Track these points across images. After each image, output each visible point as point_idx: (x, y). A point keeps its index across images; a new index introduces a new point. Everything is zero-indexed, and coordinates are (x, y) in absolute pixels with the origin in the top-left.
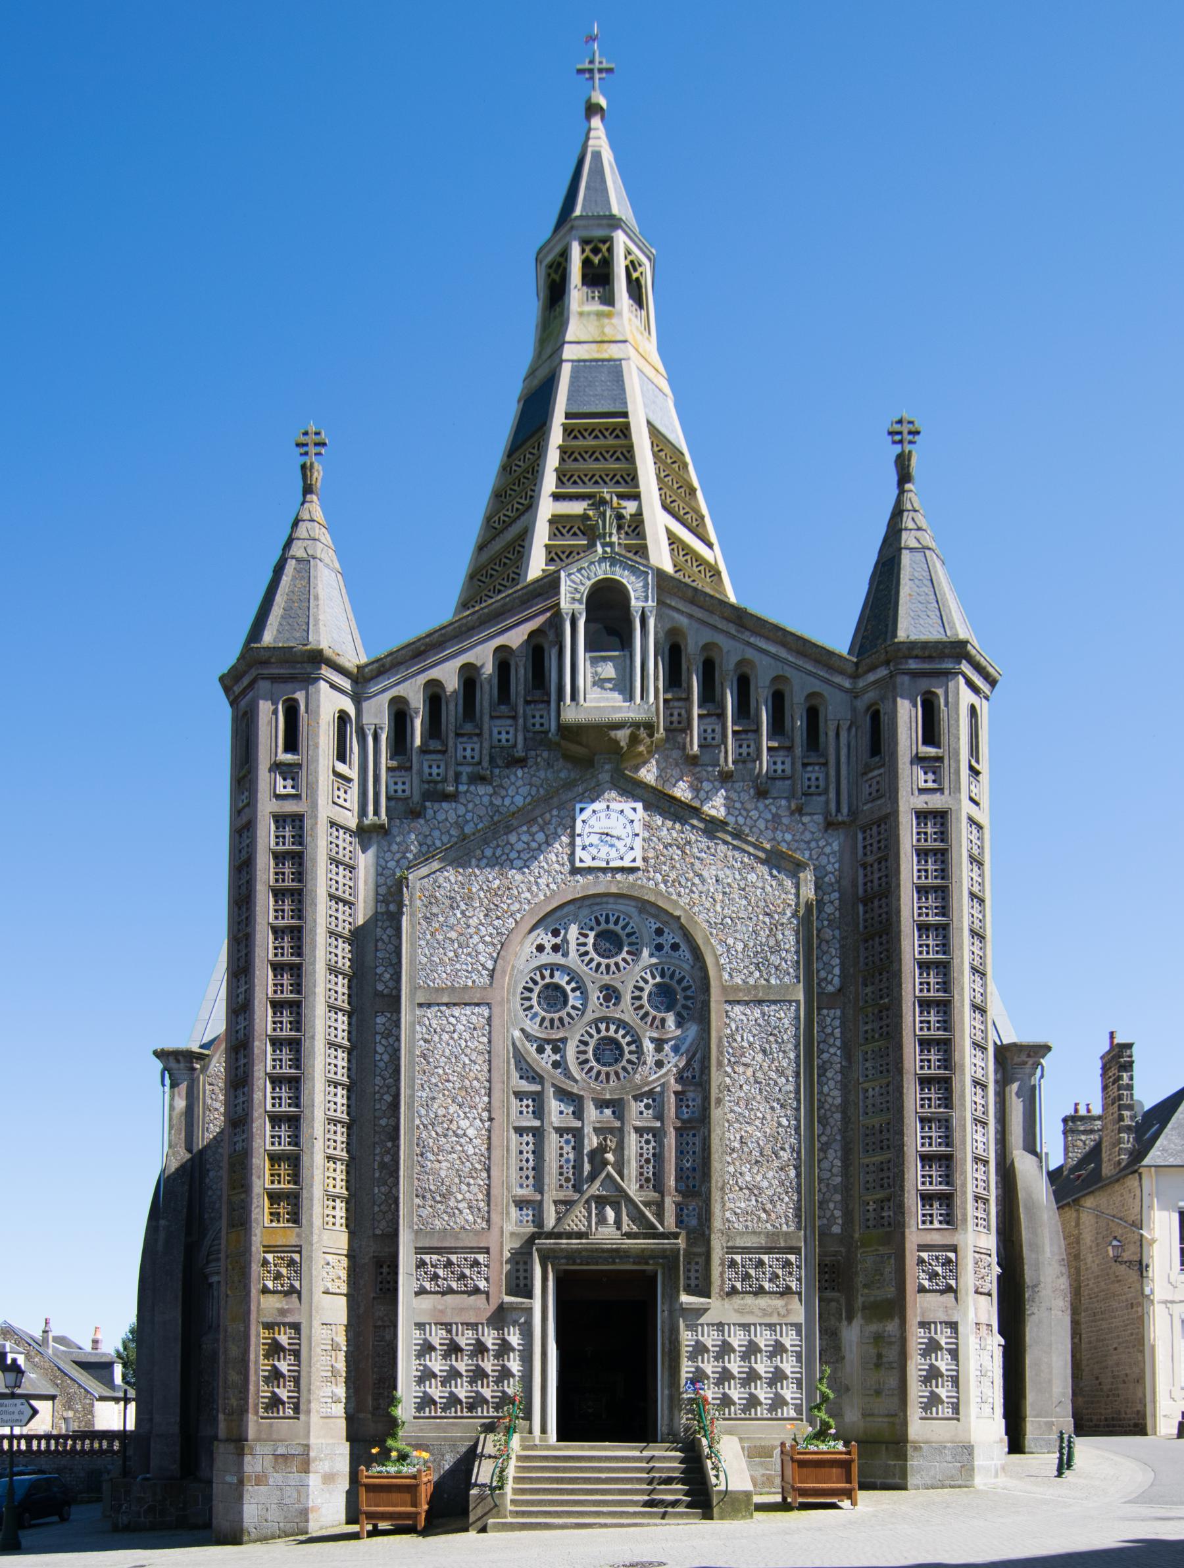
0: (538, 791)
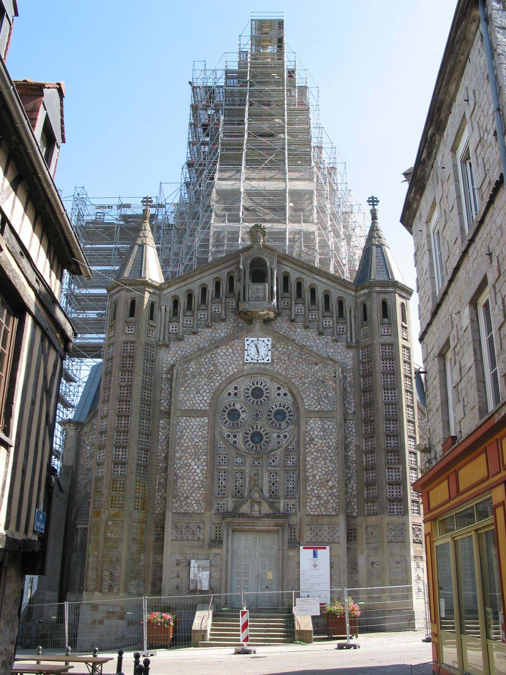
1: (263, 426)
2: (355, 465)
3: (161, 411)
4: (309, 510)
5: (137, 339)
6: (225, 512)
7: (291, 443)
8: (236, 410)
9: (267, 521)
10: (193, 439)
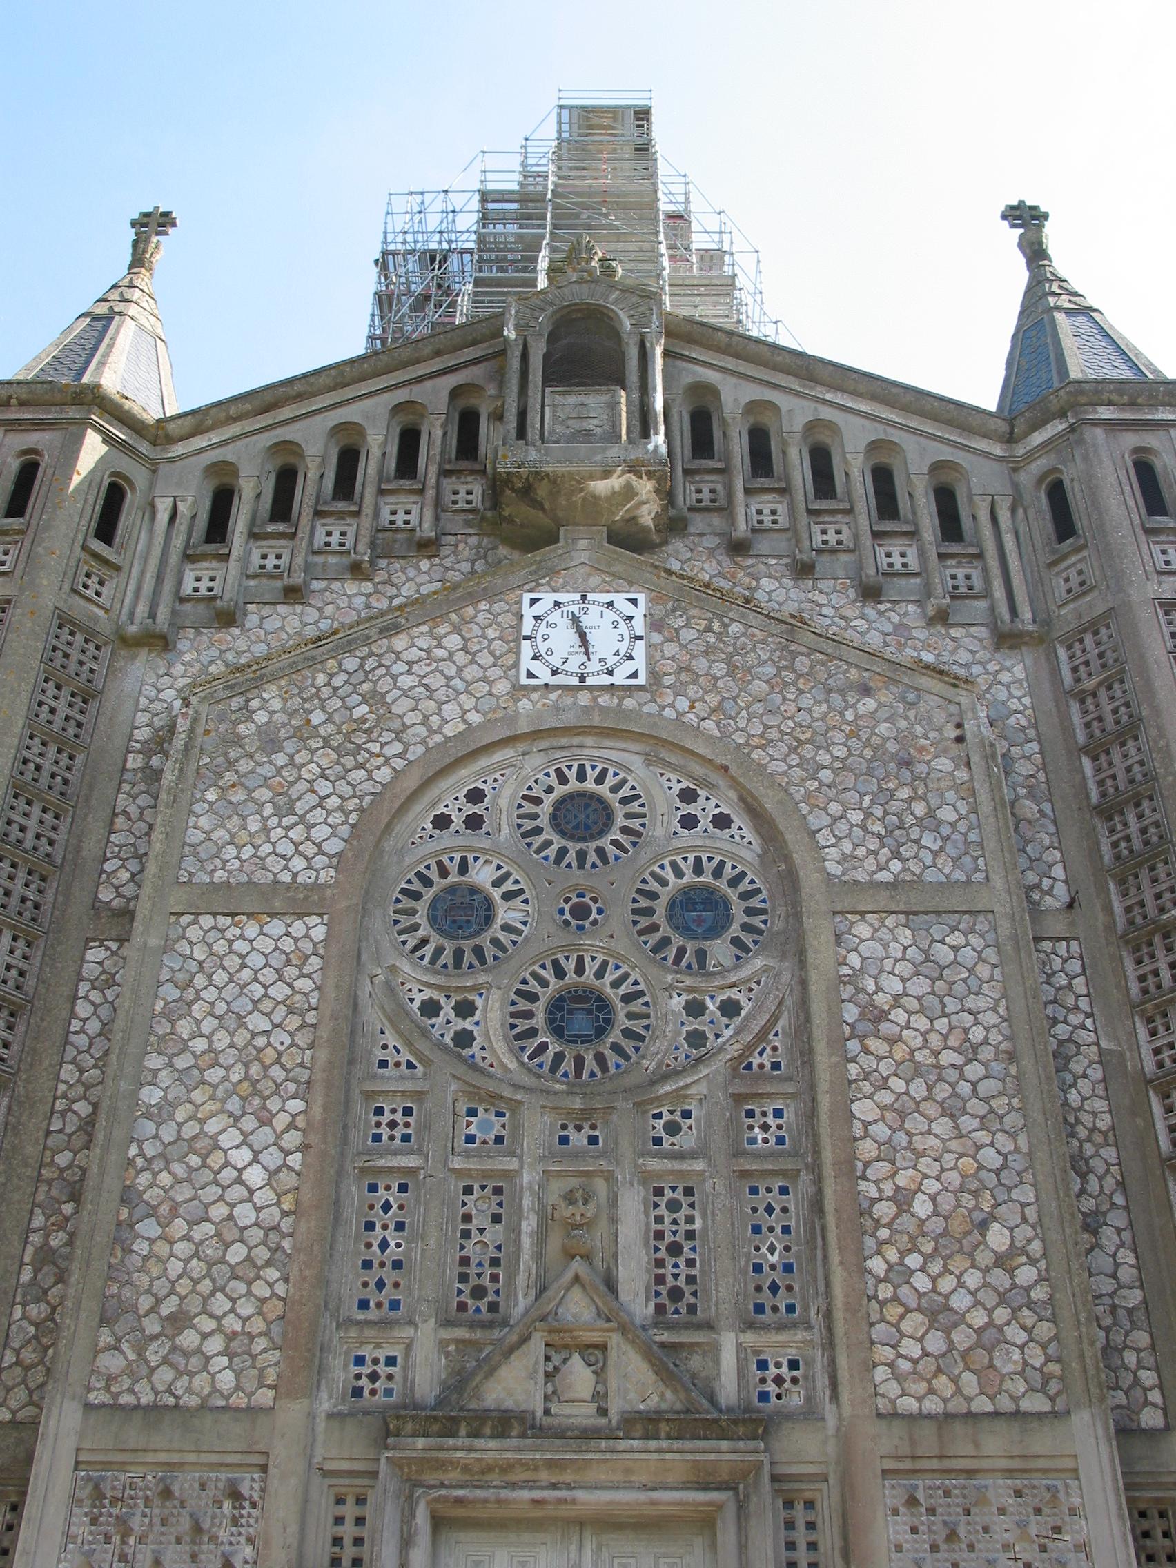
1: (610, 954)
2: (1110, 1153)
3: (97, 907)
4: (893, 1389)
5: (21, 590)
6: (396, 1407)
7: (762, 1036)
8: (474, 890)
9: (640, 1454)
10: (239, 1017)
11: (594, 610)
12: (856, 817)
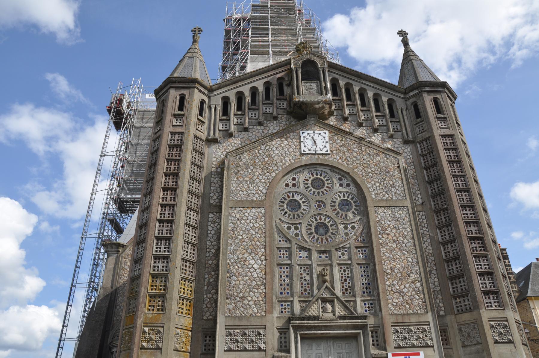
0: (234, 187)
2: (432, 258)
3: (210, 205)
11: (317, 135)
12: (377, 185)
